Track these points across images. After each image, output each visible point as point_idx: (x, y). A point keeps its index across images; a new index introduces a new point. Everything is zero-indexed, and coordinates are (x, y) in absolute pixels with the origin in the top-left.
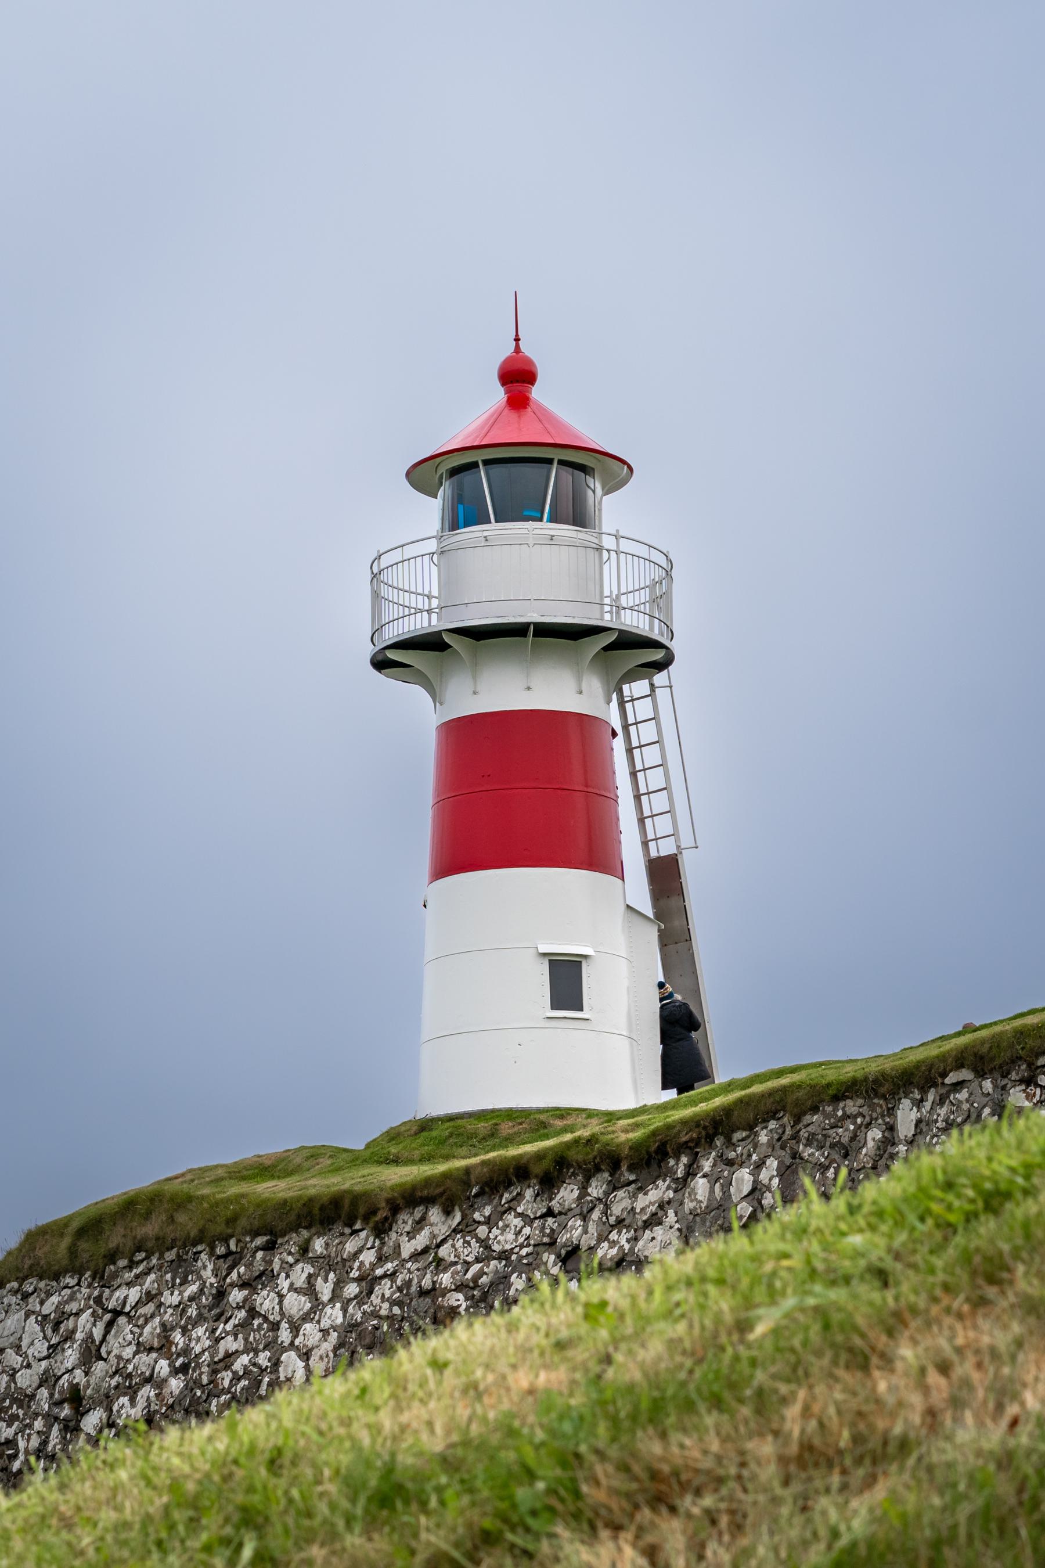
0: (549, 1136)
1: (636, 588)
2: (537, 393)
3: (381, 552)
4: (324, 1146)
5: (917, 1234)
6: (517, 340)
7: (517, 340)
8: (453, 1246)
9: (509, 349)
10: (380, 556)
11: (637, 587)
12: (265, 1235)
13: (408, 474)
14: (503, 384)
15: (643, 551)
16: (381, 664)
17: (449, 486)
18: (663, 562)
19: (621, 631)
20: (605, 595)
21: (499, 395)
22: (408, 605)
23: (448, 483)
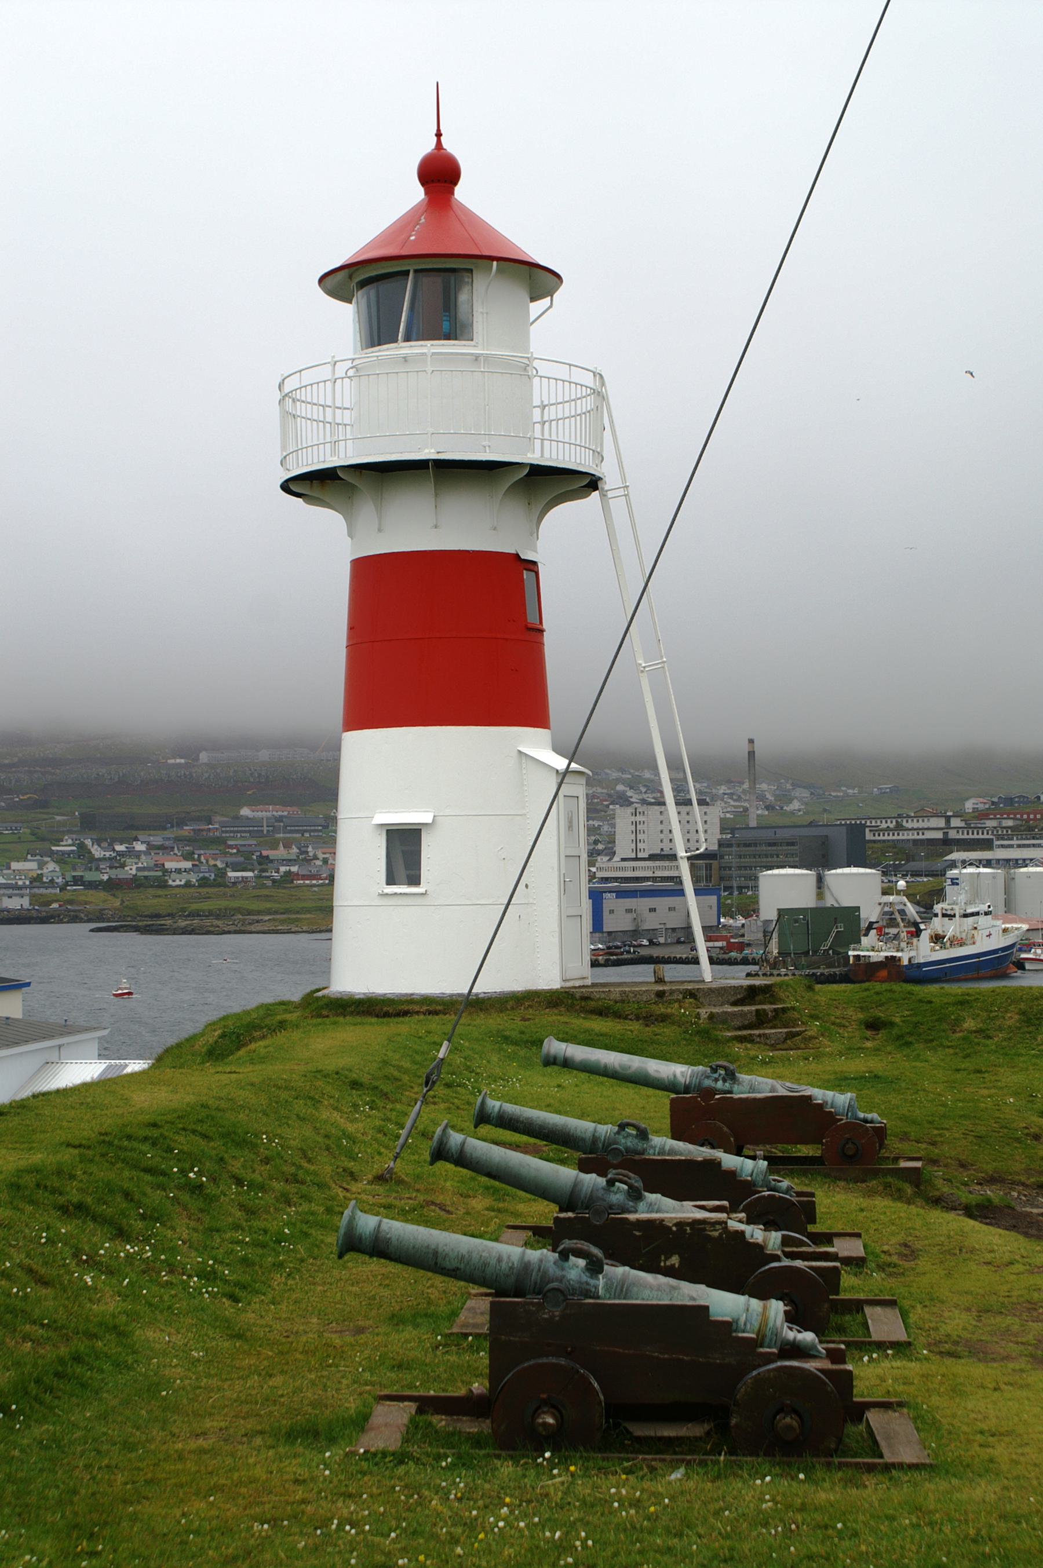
0: (328, 957)
1: (572, 398)
2: (462, 193)
3: (286, 375)
4: (473, 1236)
5: (125, 904)
6: (439, 135)
7: (439, 135)
8: (492, 1218)
9: (430, 146)
10: (283, 380)
11: (573, 397)
12: (150, 1059)
13: (321, 280)
14: (423, 184)
15: (562, 372)
16: (286, 487)
17: (363, 297)
18: (589, 380)
19: (532, 466)
20: (534, 405)
21: (417, 193)
22: (323, 403)
23: (360, 293)
